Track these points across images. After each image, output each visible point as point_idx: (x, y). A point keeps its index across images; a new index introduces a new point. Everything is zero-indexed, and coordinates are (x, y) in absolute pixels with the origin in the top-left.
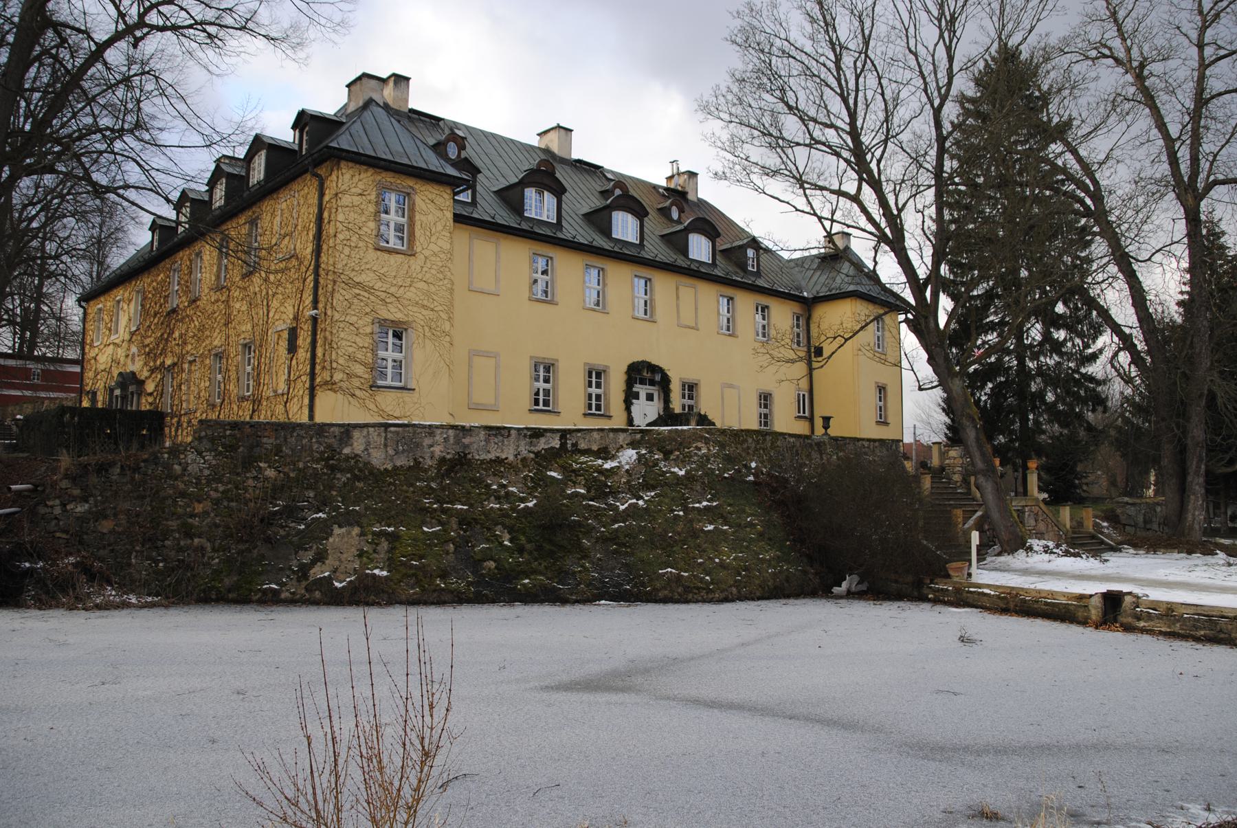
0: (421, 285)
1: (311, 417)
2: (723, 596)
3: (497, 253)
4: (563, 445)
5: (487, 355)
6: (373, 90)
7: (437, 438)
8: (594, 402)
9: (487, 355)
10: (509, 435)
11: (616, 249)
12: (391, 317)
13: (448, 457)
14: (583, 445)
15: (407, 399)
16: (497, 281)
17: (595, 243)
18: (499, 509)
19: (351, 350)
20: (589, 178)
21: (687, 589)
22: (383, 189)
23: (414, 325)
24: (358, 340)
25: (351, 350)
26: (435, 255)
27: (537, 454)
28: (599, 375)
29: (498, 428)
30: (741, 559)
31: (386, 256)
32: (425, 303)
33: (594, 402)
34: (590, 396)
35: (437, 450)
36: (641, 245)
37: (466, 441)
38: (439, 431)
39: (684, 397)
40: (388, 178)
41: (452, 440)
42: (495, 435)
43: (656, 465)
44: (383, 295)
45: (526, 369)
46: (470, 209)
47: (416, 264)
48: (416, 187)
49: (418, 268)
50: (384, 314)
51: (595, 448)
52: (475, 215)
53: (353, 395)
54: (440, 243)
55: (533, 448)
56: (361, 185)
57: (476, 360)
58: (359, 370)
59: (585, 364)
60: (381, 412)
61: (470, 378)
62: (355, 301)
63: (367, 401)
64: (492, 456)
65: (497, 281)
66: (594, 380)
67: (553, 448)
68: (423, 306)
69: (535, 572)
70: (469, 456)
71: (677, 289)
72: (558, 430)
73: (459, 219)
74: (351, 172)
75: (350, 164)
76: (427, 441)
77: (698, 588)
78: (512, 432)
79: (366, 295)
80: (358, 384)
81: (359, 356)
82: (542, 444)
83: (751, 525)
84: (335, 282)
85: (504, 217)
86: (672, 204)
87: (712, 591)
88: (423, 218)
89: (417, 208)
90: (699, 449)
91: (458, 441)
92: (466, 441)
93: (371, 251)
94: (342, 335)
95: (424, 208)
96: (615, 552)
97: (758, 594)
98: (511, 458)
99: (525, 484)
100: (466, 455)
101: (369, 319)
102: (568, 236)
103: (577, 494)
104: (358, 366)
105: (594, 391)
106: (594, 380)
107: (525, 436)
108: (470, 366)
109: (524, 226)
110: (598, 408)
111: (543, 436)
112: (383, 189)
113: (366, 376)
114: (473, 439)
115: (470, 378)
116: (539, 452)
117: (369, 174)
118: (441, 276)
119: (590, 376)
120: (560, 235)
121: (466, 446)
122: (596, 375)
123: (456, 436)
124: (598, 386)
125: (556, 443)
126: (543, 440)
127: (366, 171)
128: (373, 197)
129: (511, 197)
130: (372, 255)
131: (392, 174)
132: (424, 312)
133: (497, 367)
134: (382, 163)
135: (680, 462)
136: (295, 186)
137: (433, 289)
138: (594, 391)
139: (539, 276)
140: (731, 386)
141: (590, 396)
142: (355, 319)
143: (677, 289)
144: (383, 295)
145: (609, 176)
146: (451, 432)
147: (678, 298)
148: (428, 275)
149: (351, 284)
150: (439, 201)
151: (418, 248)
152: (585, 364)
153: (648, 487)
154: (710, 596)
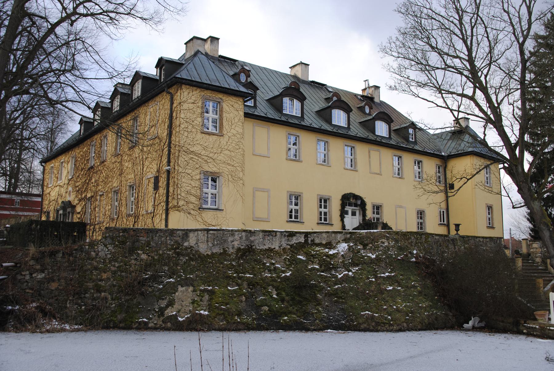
0: (227, 152)
1: (166, 225)
2: (398, 328)
3: (268, 133)
4: (306, 241)
5: (263, 190)
7: (236, 237)
8: (323, 217)
9: (263, 190)
11: (334, 130)
12: (210, 170)
13: (242, 247)
14: (317, 241)
15: (219, 215)
17: (322, 128)
19: (188, 188)
21: (378, 324)
23: (223, 174)
24: (192, 183)
25: (188, 188)
26: (234, 135)
27: (292, 246)
28: (325, 201)
29: (270, 231)
30: (409, 307)
31: (207, 136)
32: (229, 162)
33: (323, 217)
36: (349, 128)
37: (252, 238)
38: (237, 233)
40: (208, 93)
41: (244, 238)
42: (268, 235)
44: (206, 158)
47: (224, 140)
48: (224, 98)
49: (225, 143)
50: (206, 168)
51: (324, 242)
53: (189, 213)
54: (237, 129)
55: (289, 243)
56: (193, 98)
58: (193, 199)
60: (205, 222)
62: (191, 161)
63: (197, 217)
64: (266, 247)
66: (323, 204)
67: (300, 242)
68: (228, 164)
69: (291, 313)
70: (254, 247)
71: (369, 152)
72: (303, 233)
74: (188, 91)
76: (230, 239)
77: (384, 323)
78: (278, 233)
79: (197, 158)
80: (192, 207)
82: (294, 240)
84: (179, 151)
85: (272, 114)
86: (365, 105)
87: (392, 325)
88: (228, 115)
89: (224, 110)
92: (252, 238)
94: (183, 180)
95: (228, 110)
96: (336, 302)
98: (277, 248)
99: (285, 263)
100: (252, 246)
101: (198, 171)
103: (314, 269)
104: (192, 197)
106: (323, 204)
107: (285, 236)
109: (283, 119)
110: (325, 219)
111: (295, 236)
112: (205, 100)
113: (197, 203)
114: (256, 238)
117: (198, 91)
118: (237, 147)
119: (321, 202)
120: (303, 123)
122: (324, 201)
123: (246, 236)
125: (302, 240)
126: (295, 238)
127: (196, 90)
128: (200, 104)
129: (275, 102)
130: (200, 136)
132: (229, 167)
133: (269, 197)
135: (373, 251)
137: (233, 154)
138: (323, 210)
140: (401, 207)
141: (321, 213)
143: (369, 152)
144: (206, 158)
146: (244, 234)
148: (230, 147)
150: (236, 106)
152: (288, 192)
153: (354, 264)
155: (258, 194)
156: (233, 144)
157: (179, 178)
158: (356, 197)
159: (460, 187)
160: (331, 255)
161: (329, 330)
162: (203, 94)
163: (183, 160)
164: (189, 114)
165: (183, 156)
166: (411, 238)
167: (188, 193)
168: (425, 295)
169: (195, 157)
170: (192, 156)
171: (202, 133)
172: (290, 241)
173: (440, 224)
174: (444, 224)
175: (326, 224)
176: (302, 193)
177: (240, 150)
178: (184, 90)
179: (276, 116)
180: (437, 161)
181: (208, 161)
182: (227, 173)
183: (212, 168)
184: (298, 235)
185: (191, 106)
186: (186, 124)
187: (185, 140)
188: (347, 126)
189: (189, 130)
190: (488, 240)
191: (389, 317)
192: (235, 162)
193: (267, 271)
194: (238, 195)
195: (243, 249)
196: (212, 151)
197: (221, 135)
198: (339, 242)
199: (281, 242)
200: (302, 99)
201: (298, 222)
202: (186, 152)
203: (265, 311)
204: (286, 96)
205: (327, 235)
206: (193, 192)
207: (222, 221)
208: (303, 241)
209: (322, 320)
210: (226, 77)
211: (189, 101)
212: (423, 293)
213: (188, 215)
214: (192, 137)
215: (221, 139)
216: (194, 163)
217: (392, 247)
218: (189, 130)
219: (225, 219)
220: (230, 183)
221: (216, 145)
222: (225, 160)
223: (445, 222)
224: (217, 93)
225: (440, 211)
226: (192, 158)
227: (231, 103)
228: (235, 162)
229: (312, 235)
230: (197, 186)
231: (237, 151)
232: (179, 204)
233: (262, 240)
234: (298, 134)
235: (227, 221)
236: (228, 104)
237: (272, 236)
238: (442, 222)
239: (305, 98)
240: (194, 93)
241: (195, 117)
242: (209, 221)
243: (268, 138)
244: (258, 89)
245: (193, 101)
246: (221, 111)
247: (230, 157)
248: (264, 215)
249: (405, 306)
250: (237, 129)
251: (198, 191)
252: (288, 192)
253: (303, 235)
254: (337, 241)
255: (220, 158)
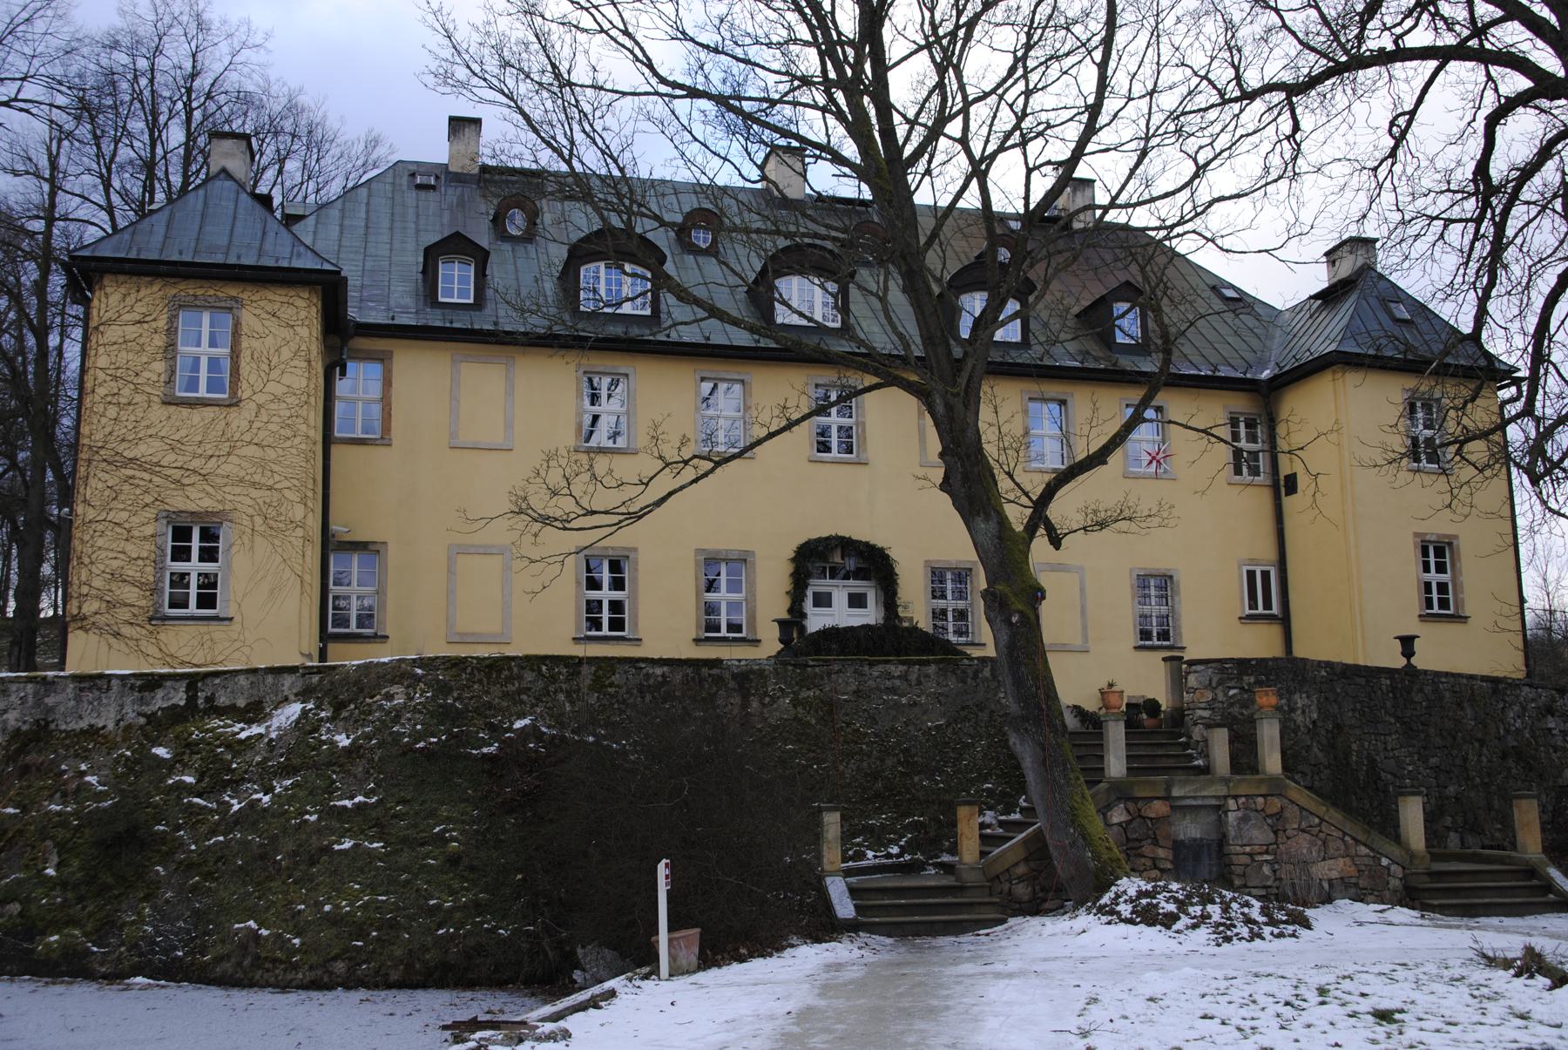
0: (251, 451)
2: (310, 976)
4: (191, 699)
6: (227, 155)
7: (13, 698)
8: (1435, 596)
10: (109, 689)
12: (192, 507)
13: (24, 728)
14: (223, 700)
15: (216, 635)
16: (509, 425)
18: (59, 814)
19: (115, 564)
21: (258, 962)
22: (177, 306)
23: (236, 515)
24: (129, 547)
25: (115, 564)
26: (277, 399)
27: (150, 717)
28: (1440, 552)
29: (91, 677)
30: (379, 907)
31: (185, 411)
32: (257, 478)
33: (1435, 596)
34: (1428, 586)
37: (50, 701)
38: (14, 687)
40: (189, 289)
42: (90, 689)
43: (316, 730)
44: (177, 474)
47: (239, 420)
48: (245, 296)
49: (244, 425)
50: (178, 502)
51: (241, 703)
53: (117, 635)
54: (286, 379)
55: (145, 709)
56: (141, 308)
57: (462, 560)
58: (130, 594)
59: (698, 551)
60: (167, 658)
62: (126, 487)
63: (143, 643)
64: (83, 724)
65: (509, 425)
66: (1432, 559)
67: (175, 706)
68: (254, 484)
69: (73, 922)
70: (53, 726)
74: (123, 290)
75: (121, 278)
77: (275, 961)
78: (114, 682)
79: (147, 476)
80: (127, 616)
81: (130, 572)
82: (158, 701)
83: (441, 839)
84: (89, 461)
87: (295, 967)
88: (256, 344)
89: (245, 329)
90: (389, 697)
91: (39, 702)
92: (50, 701)
93: (155, 407)
94: (100, 542)
95: (259, 328)
96: (195, 888)
97: (394, 976)
98: (111, 726)
99: (114, 769)
100: (47, 723)
101: (150, 514)
103: (180, 785)
104: (128, 588)
105: (1434, 577)
106: (1432, 559)
107: (132, 688)
108: (451, 571)
110: (1444, 604)
111: (160, 686)
112: (177, 306)
113: (143, 603)
114: (59, 698)
116: (154, 714)
117: (155, 288)
118: (289, 433)
119: (1425, 553)
121: (51, 710)
123: (36, 694)
124: (1441, 568)
125: (180, 698)
126: (160, 693)
127: (151, 283)
128: (162, 323)
130: (158, 412)
131: (199, 283)
132: (255, 493)
134: (163, 268)
135: (350, 726)
137: (271, 454)
138: (1434, 577)
141: (1428, 586)
142: (125, 515)
144: (177, 474)
148: (262, 434)
149: (119, 462)
150: (287, 313)
151: (245, 392)
153: (286, 770)
154: (289, 977)
156: (273, 427)
157: (86, 538)
158: (846, 545)
159: (670, 494)
160: (241, 742)
161: (139, 979)
162: (173, 291)
163: (100, 485)
164: (124, 353)
165: (101, 475)
166: (520, 678)
167: (116, 576)
168: (472, 868)
169: (138, 474)
170: (129, 472)
171: (164, 403)
172: (148, 704)
173: (1249, 617)
174: (1272, 617)
175: (735, 639)
177: (297, 440)
178: (109, 290)
180: (1240, 403)
181: (186, 481)
182: (250, 511)
183: (196, 500)
184: (168, 684)
185: (132, 331)
186: (113, 384)
187: (108, 430)
189: (123, 400)
191: (296, 941)
192: (277, 478)
193: (58, 795)
194: (288, 572)
195: (26, 733)
196: (199, 451)
197: (234, 403)
198: (286, 699)
199: (122, 706)
201: (623, 639)
202: (109, 463)
203: (11, 917)
205: (252, 678)
206: (130, 573)
207: (226, 653)
208: (182, 703)
209: (136, 945)
211: (127, 317)
212: (466, 861)
213: (112, 640)
214: (133, 418)
215: (230, 418)
216: (138, 491)
217: (415, 710)
218: (123, 400)
219: (237, 645)
220: (258, 539)
221: (213, 435)
222: (242, 473)
223: (1275, 610)
224: (221, 284)
225: (1251, 574)
226: (133, 477)
227: (269, 308)
228: (277, 478)
229: (208, 681)
230: (145, 554)
231: (288, 443)
232: (84, 610)
233: (72, 703)
234: (622, 371)
235: (246, 650)
236: (257, 312)
237: (99, 689)
238: (1261, 610)
240: (142, 294)
241: (145, 359)
242: (183, 654)
245: (138, 318)
246: (236, 334)
247: (262, 464)
249: (365, 907)
250: (286, 379)
251: (149, 569)
253: (184, 684)
254: (280, 698)
255: (227, 468)
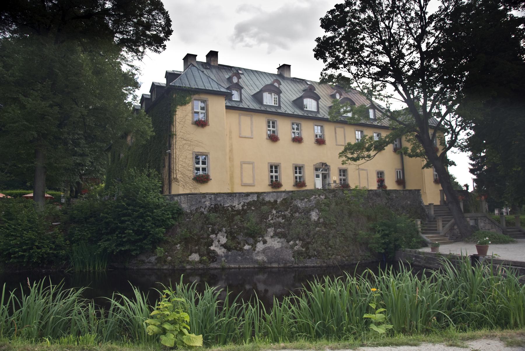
1: (170, 193)
3: (251, 120)
5: (249, 163)
7: (207, 198)
9: (249, 163)
11: (305, 115)
16: (252, 132)
17: (295, 113)
20: (295, 85)
28: (300, 168)
35: (208, 203)
36: (318, 112)
37: (219, 199)
38: (207, 196)
39: (340, 175)
41: (213, 199)
45: (267, 169)
46: (238, 104)
52: (241, 106)
61: (241, 173)
65: (252, 132)
71: (335, 129)
72: (256, 193)
73: (227, 107)
76: (203, 200)
82: (250, 199)
85: (254, 106)
86: (336, 93)
91: (215, 199)
102: (283, 111)
109: (263, 108)
115: (241, 173)
120: (279, 111)
122: (298, 169)
123: (215, 197)
125: (255, 198)
129: (258, 97)
133: (253, 168)
136: (236, 111)
139: (295, 131)
140: (245, 163)
143: (335, 129)
145: (309, 83)
146: (212, 196)
147: (336, 133)
152: (269, 163)
155: (244, 166)
176: (304, 165)
179: (298, 112)
188: (239, 100)
190: (407, 192)
200: (317, 98)
204: (265, 91)
210: (211, 82)
239: (281, 92)
243: (252, 124)
244: (242, 88)
248: (250, 181)
252: (269, 163)
